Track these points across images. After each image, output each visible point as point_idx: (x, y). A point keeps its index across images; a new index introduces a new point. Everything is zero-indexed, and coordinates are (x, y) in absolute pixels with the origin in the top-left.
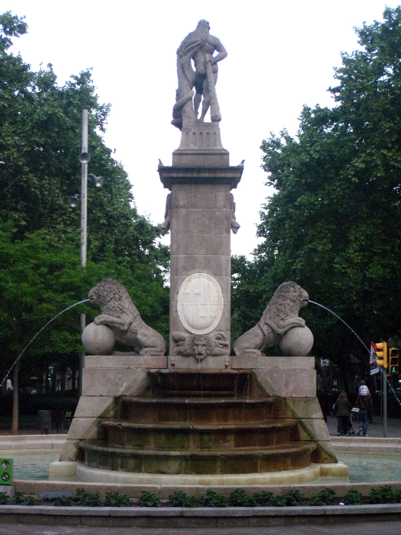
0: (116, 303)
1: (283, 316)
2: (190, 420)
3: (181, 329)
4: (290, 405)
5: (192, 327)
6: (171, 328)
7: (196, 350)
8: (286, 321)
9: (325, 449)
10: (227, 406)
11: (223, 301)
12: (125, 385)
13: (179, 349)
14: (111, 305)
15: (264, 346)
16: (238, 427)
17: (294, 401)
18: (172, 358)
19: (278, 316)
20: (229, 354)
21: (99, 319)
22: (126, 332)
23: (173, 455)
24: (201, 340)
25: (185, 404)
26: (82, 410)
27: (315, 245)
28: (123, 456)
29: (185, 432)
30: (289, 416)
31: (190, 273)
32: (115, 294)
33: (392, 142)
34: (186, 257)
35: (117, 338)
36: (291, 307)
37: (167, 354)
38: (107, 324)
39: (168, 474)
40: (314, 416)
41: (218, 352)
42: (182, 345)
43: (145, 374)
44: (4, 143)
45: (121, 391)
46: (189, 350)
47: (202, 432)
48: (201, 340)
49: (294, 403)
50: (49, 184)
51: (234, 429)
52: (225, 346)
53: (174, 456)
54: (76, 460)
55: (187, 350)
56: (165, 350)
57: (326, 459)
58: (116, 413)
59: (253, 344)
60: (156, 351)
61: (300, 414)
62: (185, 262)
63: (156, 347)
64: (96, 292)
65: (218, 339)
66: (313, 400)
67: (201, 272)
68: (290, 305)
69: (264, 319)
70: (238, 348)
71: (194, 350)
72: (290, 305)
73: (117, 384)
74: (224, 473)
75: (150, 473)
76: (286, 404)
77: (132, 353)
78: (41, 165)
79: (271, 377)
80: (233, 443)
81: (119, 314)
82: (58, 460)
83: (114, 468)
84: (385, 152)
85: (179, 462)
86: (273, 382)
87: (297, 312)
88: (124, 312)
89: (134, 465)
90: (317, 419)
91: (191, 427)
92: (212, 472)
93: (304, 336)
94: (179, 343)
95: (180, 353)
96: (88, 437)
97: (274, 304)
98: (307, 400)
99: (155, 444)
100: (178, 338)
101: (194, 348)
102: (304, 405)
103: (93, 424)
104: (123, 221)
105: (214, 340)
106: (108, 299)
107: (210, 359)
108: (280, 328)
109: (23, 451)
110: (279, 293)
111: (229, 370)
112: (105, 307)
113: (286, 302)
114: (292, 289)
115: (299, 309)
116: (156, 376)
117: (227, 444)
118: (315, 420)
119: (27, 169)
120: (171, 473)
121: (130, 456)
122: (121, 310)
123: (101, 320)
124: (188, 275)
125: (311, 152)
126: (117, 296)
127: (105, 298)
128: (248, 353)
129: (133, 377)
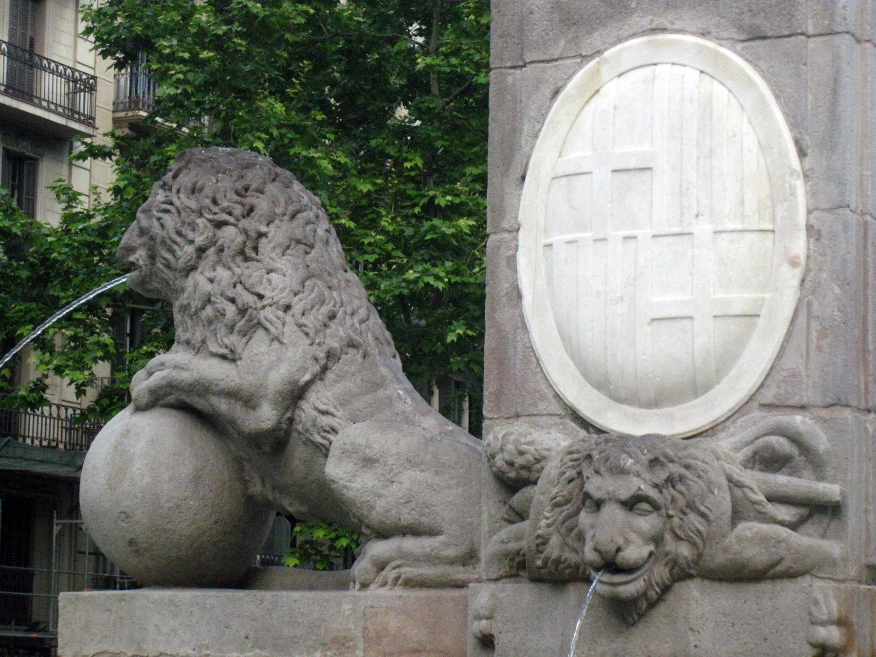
0: (222, 274)
3: (542, 406)
5: (601, 384)
7: (589, 535)
14: (196, 286)
21: (150, 374)
24: (622, 472)
31: (596, 39)
38: (189, 405)
41: (756, 555)
48: (622, 472)
60: (431, 559)
63: (432, 532)
65: (769, 461)
67: (664, 30)
81: (233, 340)
100: (511, 464)
122: (242, 312)
124: (585, 58)
126: (230, 235)
127: (172, 252)
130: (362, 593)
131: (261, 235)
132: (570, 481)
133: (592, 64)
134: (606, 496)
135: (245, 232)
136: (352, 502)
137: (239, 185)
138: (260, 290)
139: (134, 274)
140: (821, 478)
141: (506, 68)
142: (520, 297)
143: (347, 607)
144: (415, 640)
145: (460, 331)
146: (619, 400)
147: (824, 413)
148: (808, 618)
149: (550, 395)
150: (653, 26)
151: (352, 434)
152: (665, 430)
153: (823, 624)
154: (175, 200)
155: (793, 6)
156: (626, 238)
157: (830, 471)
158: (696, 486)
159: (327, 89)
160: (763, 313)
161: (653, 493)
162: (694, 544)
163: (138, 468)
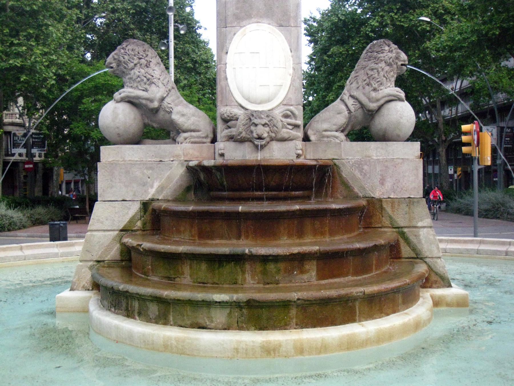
0: (143, 71)
1: (376, 86)
2: (247, 237)
3: (233, 104)
4: (387, 209)
5: (248, 100)
6: (218, 104)
7: (255, 131)
8: (380, 91)
9: (434, 269)
10: (303, 214)
11: (292, 62)
12: (156, 185)
13: (231, 132)
14: (134, 73)
15: (349, 128)
16: (323, 248)
17: (393, 203)
18: (220, 145)
19: (368, 85)
20: (301, 139)
21: (120, 94)
22: (156, 111)
23: (218, 300)
25: (238, 213)
26: (99, 220)
27: (343, 83)
28: (141, 298)
29: (237, 259)
30: (386, 225)
31: (244, 23)
32: (140, 59)
33: (397, 9)
35: (146, 121)
36: (387, 72)
37: (214, 140)
38: (132, 102)
39: (210, 329)
40: (420, 224)
41: (286, 136)
42: (234, 126)
43: (184, 168)
44: (115, 8)
45: (150, 193)
46: (244, 133)
47: (265, 259)
48: (262, 118)
49: (393, 207)
50: (151, 39)
51: (316, 253)
52: (296, 126)
53: (220, 302)
54: (92, 290)
55: (241, 133)
56: (211, 136)
57: (436, 282)
58: (144, 224)
59: (334, 125)
60: (198, 137)
61: (401, 222)
62: (237, 9)
63: (198, 131)
64: (116, 57)
65: (286, 116)
66: (418, 202)
67: (260, 22)
68: (385, 70)
69: (348, 91)
70: (313, 130)
71: (252, 132)
72: (385, 70)
73: (144, 184)
74: (302, 328)
75: (181, 326)
76: (382, 208)
77: (167, 141)
78: (145, 25)
79: (361, 171)
80: (314, 273)
81: (147, 86)
82: (69, 289)
83: (129, 314)
84: (393, 14)
85: (228, 311)
86: (364, 178)
87: (393, 79)
88: (153, 83)
89: (157, 313)
90: (424, 227)
91: (247, 251)
92: (283, 326)
93: (402, 114)
94: (229, 124)
95: (231, 138)
96: (108, 258)
97: (364, 68)
98: (410, 201)
99: (191, 276)
100: (228, 116)
101: (251, 130)
102: (407, 209)
103: (114, 239)
104: (204, 65)
105: (279, 117)
106: (131, 65)
107: (275, 146)
108: (373, 102)
109: (70, 258)
110: (369, 54)
111: (301, 161)
112: (127, 77)
113: (380, 65)
114: (387, 48)
115: (395, 76)
116: (196, 170)
117: (305, 276)
118: (422, 229)
119: (132, 26)
120: (216, 328)
121: (150, 298)
122: (148, 80)
123: (123, 95)
124: (241, 27)
125: (339, 16)
126: (143, 61)
128: (328, 137)
129: (168, 174)
130: (181, 145)
131: (150, 61)
135: (147, 61)
136: (179, 124)
137: (144, 49)
138: (152, 74)
139: (112, 69)
140: (296, 120)
142: (227, 79)
143: (179, 148)
145: (24, 78)
146: (252, 103)
151: (176, 109)
153: (299, 150)
154: (127, 52)
157: (298, 119)
158: (275, 121)
159: (99, 21)
161: (268, 123)
162: (275, 134)
163: (121, 116)
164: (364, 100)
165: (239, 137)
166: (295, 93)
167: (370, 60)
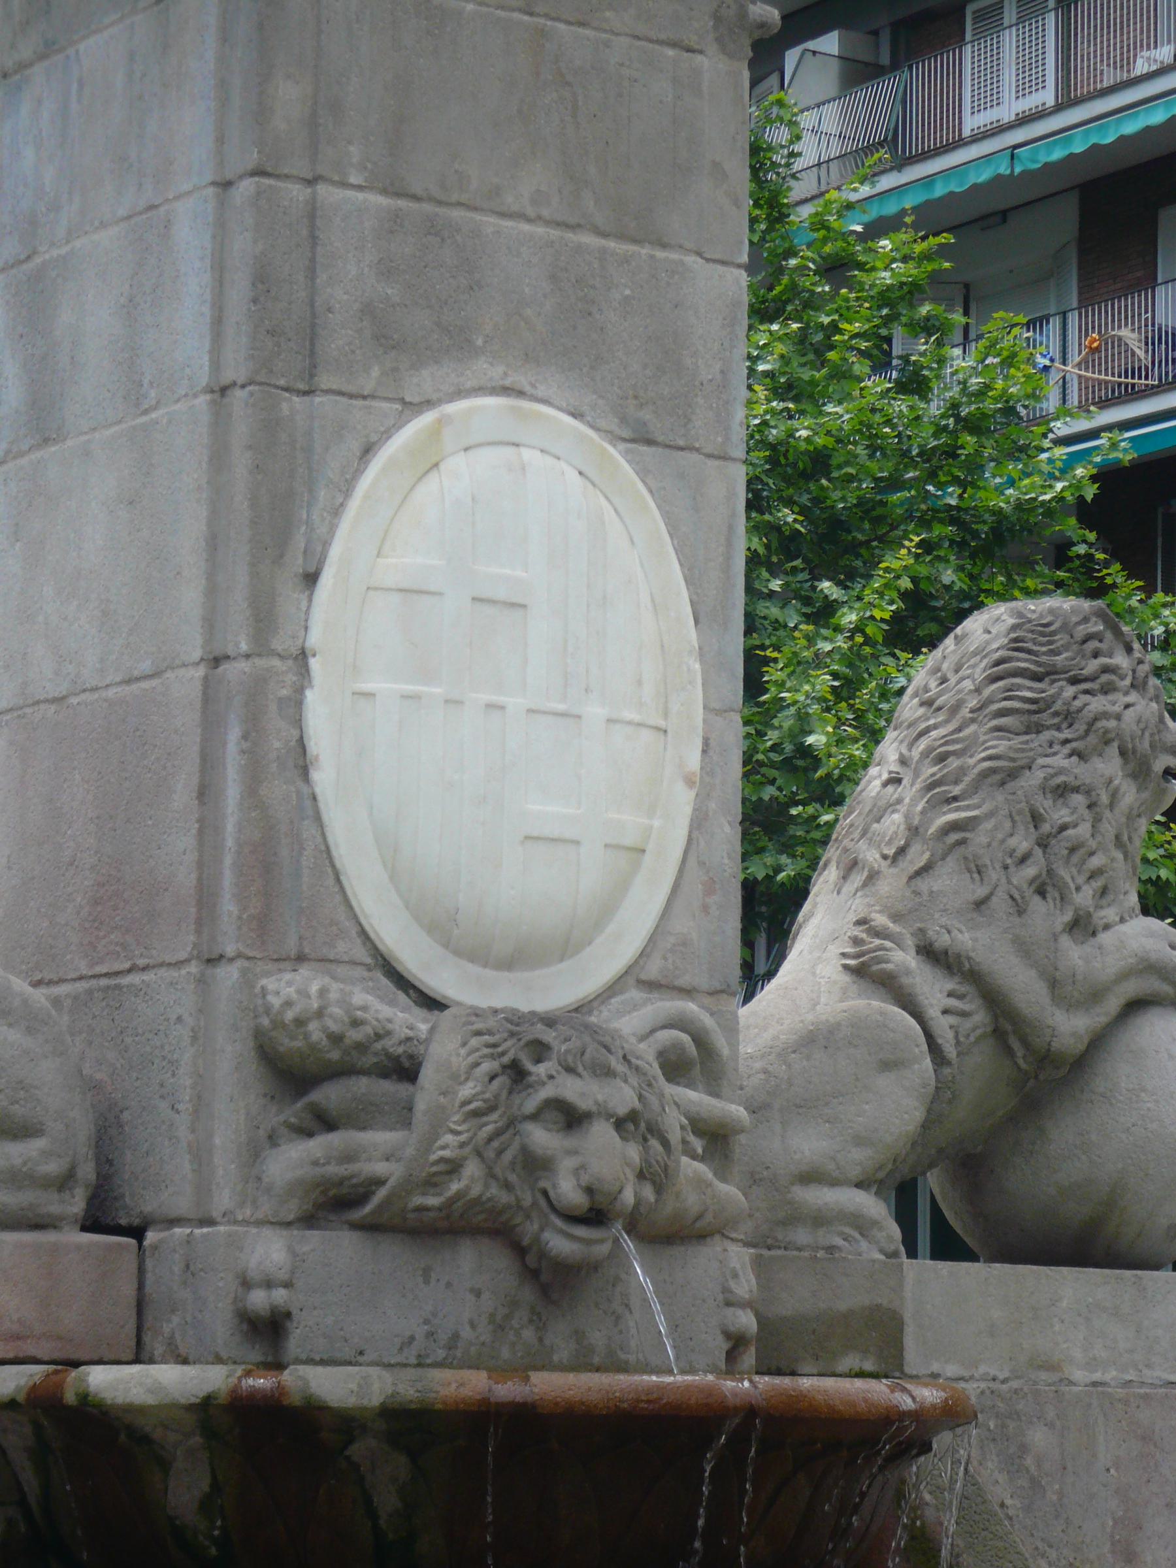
1: (1084, 898)
3: (341, 947)
8: (1104, 938)
13: (349, 1157)
31: (423, 381)
34: (396, 217)
46: (472, 1169)
55: (453, 1167)
67: (521, 394)
94: (330, 1095)
100: (336, 1039)
128: (819, 1220)
132: (492, 1078)
133: (427, 419)
134: (594, 1109)
141: (277, 387)
144: (15, 1318)
146: (458, 953)
147: (707, 1000)
148: (720, 1297)
149: (354, 932)
150: (508, 382)
152: (525, 1004)
155: (690, 406)
156: (490, 706)
160: (650, 848)
164: (1023, 984)
165: (433, 1201)
166: (705, 908)
167: (1039, 729)
